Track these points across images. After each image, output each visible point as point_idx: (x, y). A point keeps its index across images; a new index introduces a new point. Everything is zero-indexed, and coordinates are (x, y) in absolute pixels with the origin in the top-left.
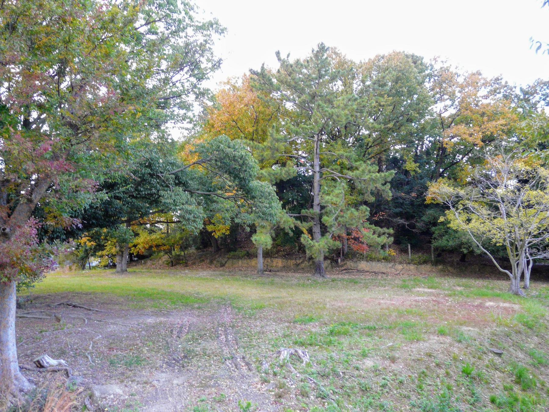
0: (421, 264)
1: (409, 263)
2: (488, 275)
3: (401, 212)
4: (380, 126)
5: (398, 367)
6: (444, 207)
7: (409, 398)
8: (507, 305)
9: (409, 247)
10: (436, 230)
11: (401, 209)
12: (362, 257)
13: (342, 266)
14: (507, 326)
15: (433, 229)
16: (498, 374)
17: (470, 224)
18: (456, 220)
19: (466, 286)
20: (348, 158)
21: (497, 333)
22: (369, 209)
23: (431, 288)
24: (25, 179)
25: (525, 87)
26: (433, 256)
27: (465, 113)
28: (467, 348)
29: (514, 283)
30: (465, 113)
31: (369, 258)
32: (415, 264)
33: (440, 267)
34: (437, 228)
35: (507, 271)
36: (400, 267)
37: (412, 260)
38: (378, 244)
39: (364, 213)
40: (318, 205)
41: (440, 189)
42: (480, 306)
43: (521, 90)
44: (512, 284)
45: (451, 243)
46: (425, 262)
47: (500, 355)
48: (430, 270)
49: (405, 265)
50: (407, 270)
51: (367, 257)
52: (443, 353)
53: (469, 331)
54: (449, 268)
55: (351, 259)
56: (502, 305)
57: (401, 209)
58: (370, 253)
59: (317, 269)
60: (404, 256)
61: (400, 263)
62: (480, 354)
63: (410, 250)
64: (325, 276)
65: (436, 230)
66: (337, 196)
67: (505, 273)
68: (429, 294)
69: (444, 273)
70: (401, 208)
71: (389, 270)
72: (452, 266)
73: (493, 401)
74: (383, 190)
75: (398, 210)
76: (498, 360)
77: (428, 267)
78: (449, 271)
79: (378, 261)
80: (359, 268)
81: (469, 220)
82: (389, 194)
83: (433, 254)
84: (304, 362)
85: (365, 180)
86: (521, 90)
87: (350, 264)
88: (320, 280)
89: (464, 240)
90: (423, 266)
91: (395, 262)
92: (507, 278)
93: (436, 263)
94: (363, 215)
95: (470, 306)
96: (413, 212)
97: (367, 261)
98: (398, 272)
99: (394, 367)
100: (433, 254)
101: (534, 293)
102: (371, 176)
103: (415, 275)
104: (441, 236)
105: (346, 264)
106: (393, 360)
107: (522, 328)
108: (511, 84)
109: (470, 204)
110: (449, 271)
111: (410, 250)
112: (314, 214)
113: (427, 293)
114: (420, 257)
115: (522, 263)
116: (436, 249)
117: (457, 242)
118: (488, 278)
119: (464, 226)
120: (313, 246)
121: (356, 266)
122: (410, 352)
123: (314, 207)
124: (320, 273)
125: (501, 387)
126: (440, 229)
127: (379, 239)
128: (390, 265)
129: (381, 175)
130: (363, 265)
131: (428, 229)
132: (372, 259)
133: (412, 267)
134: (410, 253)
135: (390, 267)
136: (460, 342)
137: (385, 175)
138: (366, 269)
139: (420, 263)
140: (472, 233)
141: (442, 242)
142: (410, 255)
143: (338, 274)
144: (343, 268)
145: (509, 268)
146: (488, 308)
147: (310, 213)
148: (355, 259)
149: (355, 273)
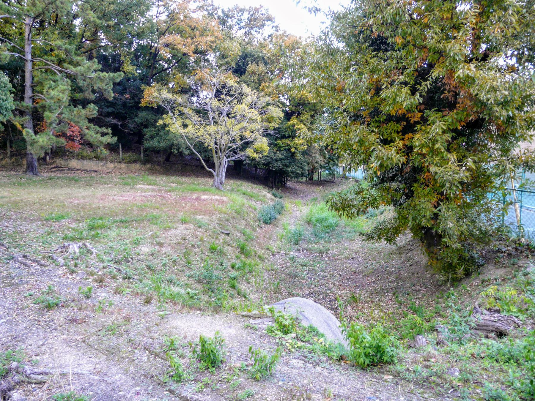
0: (131, 163)
1: (120, 162)
2: (189, 174)
3: (113, 112)
4: (101, 21)
5: (166, 250)
6: (160, 111)
7: (183, 271)
8: (217, 197)
9: (120, 146)
10: (147, 132)
11: (113, 109)
12: (72, 155)
13: (51, 164)
14: (226, 214)
15: (145, 130)
16: (230, 249)
17: (181, 128)
18: (175, 126)
19: (178, 183)
20: (67, 51)
21: (222, 219)
22: (97, 108)
23: (150, 185)
24: (91, 89)
25: (226, 10)
26: (142, 156)
27: (180, 24)
28: (206, 232)
29: (216, 180)
30: (180, 24)
31: (80, 157)
32: (125, 163)
33: (148, 166)
34: (148, 129)
35: (211, 170)
36: (111, 165)
37: (123, 159)
38: (102, 142)
39: (93, 111)
40: (30, 98)
41: (154, 94)
42: (198, 199)
43: (223, 11)
44: (215, 180)
45: (162, 144)
46: (135, 161)
47: (228, 234)
48: (139, 168)
49: (116, 164)
50: (118, 168)
51: (78, 155)
52: (192, 236)
53: (203, 219)
54: (157, 167)
55: (61, 157)
56: (213, 197)
57: (113, 109)
58: (80, 151)
59: (30, 168)
60: (115, 156)
61: (112, 162)
62: (215, 235)
63: (121, 149)
64: (38, 174)
65: (147, 132)
66: (63, 92)
67: (210, 172)
68: (153, 190)
69: (153, 172)
70: (114, 108)
71: (100, 168)
72: (159, 165)
73: (233, 267)
74: (105, 90)
75: (110, 110)
76: (228, 239)
77: (138, 166)
78: (156, 170)
79: (90, 159)
80: (70, 166)
81: (185, 126)
82: (111, 95)
83: (142, 154)
84: (94, 253)
85: (90, 78)
86: (223, 11)
87: (59, 162)
88: (35, 178)
89: (175, 142)
90: (133, 165)
91: (106, 161)
92: (211, 175)
93: (145, 162)
94: (91, 113)
95: (190, 199)
96: (125, 113)
97: (78, 159)
98: (109, 171)
99: (164, 250)
100: (142, 154)
101: (228, 187)
102: (99, 74)
103: (126, 174)
104: (152, 137)
105: (55, 162)
106: (161, 245)
107: (235, 215)
108: (216, 5)
109: (186, 111)
110: (156, 170)
111: (121, 149)
112: (27, 107)
113: (150, 189)
114: (130, 156)
115: (223, 162)
116: (146, 150)
117: (169, 143)
118: (189, 175)
119: (182, 131)
120: (36, 142)
121: (66, 163)
122: (170, 238)
123: (25, 99)
124: (32, 171)
125: (234, 257)
126: (152, 131)
127: (102, 138)
128: (102, 164)
129: (109, 76)
130: (74, 163)
131: (140, 130)
132: (83, 158)
133: (123, 166)
134: (121, 152)
135: (101, 166)
136: (200, 227)
137: (114, 76)
138: (77, 167)
139: (130, 162)
140: (187, 137)
141: (154, 143)
142: (121, 154)
143: (48, 172)
144: (52, 166)
145: (213, 166)
146: (204, 200)
147: (22, 106)
148: (65, 157)
149: (66, 171)
